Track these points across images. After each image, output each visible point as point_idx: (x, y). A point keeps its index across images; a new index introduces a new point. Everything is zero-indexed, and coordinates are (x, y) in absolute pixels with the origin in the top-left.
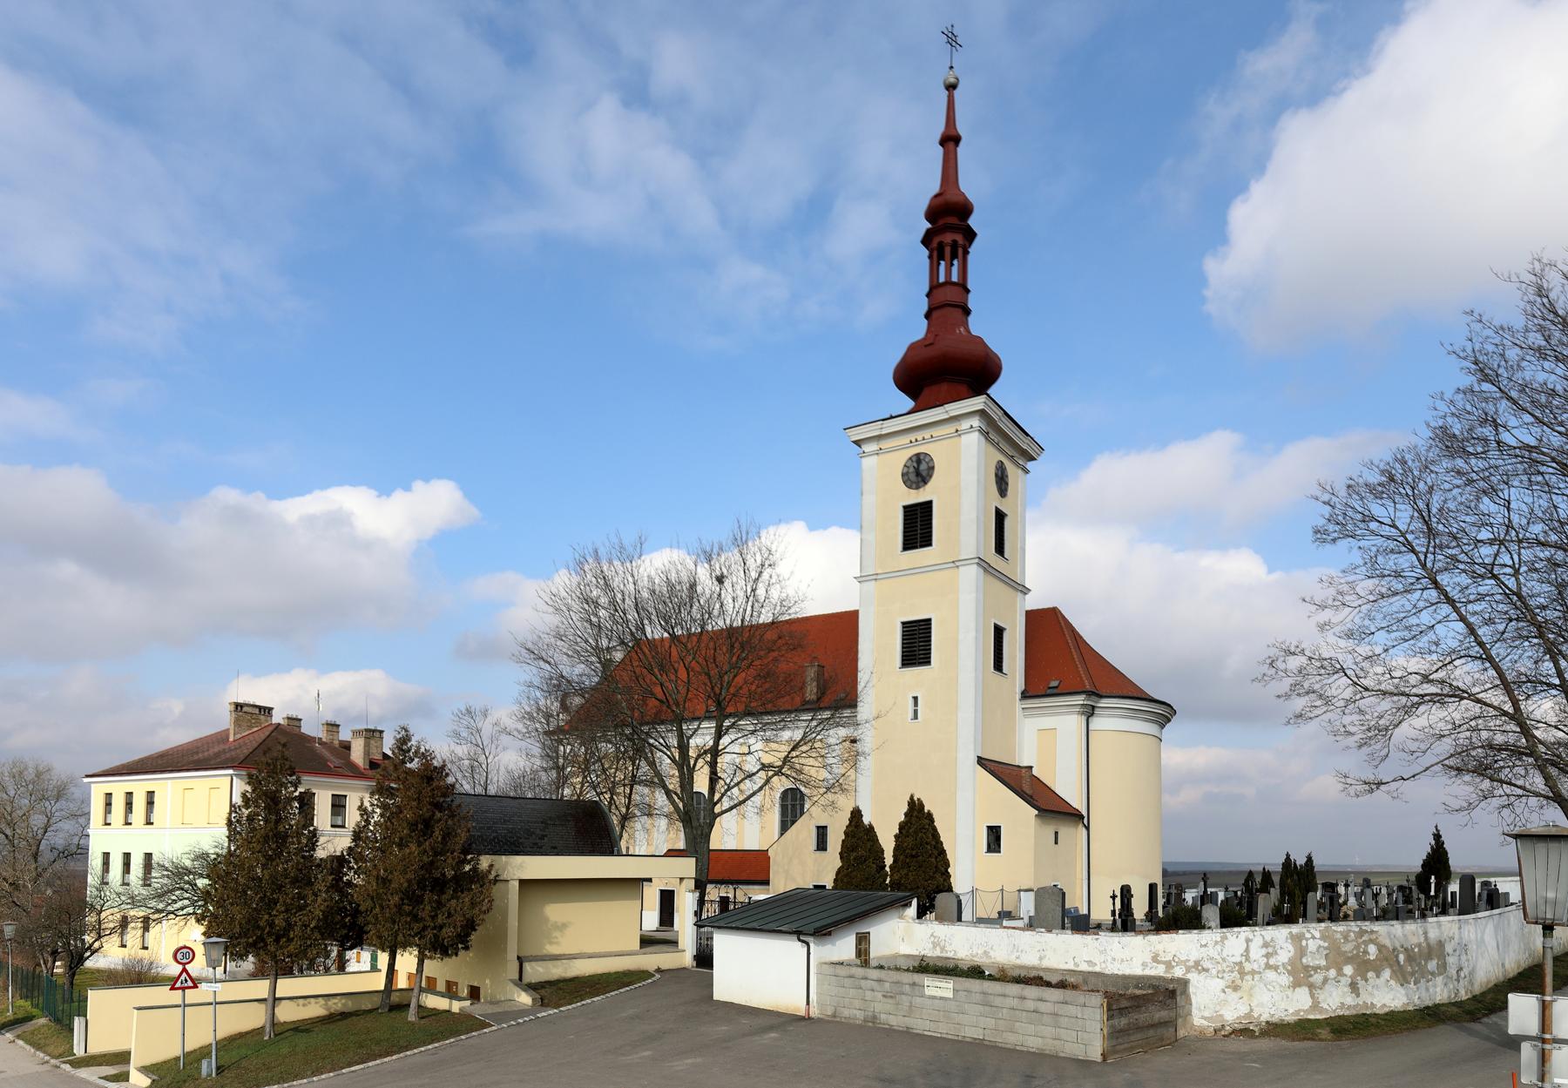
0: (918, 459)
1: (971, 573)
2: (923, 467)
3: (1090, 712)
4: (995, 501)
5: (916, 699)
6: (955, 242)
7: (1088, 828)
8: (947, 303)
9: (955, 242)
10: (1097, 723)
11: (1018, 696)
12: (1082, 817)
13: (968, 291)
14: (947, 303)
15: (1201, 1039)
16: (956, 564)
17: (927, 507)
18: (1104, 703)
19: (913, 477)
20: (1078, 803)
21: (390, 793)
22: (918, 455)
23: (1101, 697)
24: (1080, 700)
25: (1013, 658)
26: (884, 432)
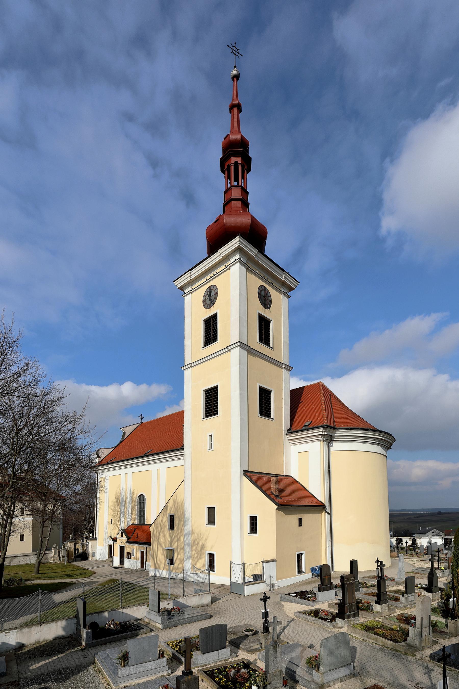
0: (210, 290)
1: (237, 352)
2: (213, 294)
3: (329, 440)
4: (257, 308)
5: (211, 436)
6: (236, 162)
7: (330, 514)
8: (237, 199)
9: (236, 162)
10: (336, 446)
11: (284, 432)
12: (324, 507)
13: (247, 193)
14: (237, 199)
15: (64, 619)
16: (228, 349)
17: (214, 317)
18: (338, 433)
19: (208, 302)
20: (321, 496)
21: (357, 582)
22: (210, 287)
23: (336, 429)
24: (320, 431)
25: (279, 409)
26: (192, 277)
